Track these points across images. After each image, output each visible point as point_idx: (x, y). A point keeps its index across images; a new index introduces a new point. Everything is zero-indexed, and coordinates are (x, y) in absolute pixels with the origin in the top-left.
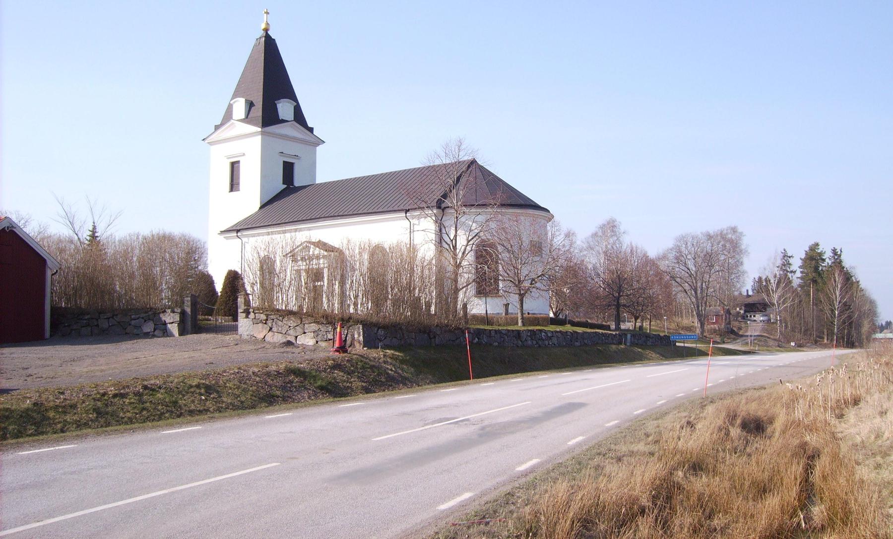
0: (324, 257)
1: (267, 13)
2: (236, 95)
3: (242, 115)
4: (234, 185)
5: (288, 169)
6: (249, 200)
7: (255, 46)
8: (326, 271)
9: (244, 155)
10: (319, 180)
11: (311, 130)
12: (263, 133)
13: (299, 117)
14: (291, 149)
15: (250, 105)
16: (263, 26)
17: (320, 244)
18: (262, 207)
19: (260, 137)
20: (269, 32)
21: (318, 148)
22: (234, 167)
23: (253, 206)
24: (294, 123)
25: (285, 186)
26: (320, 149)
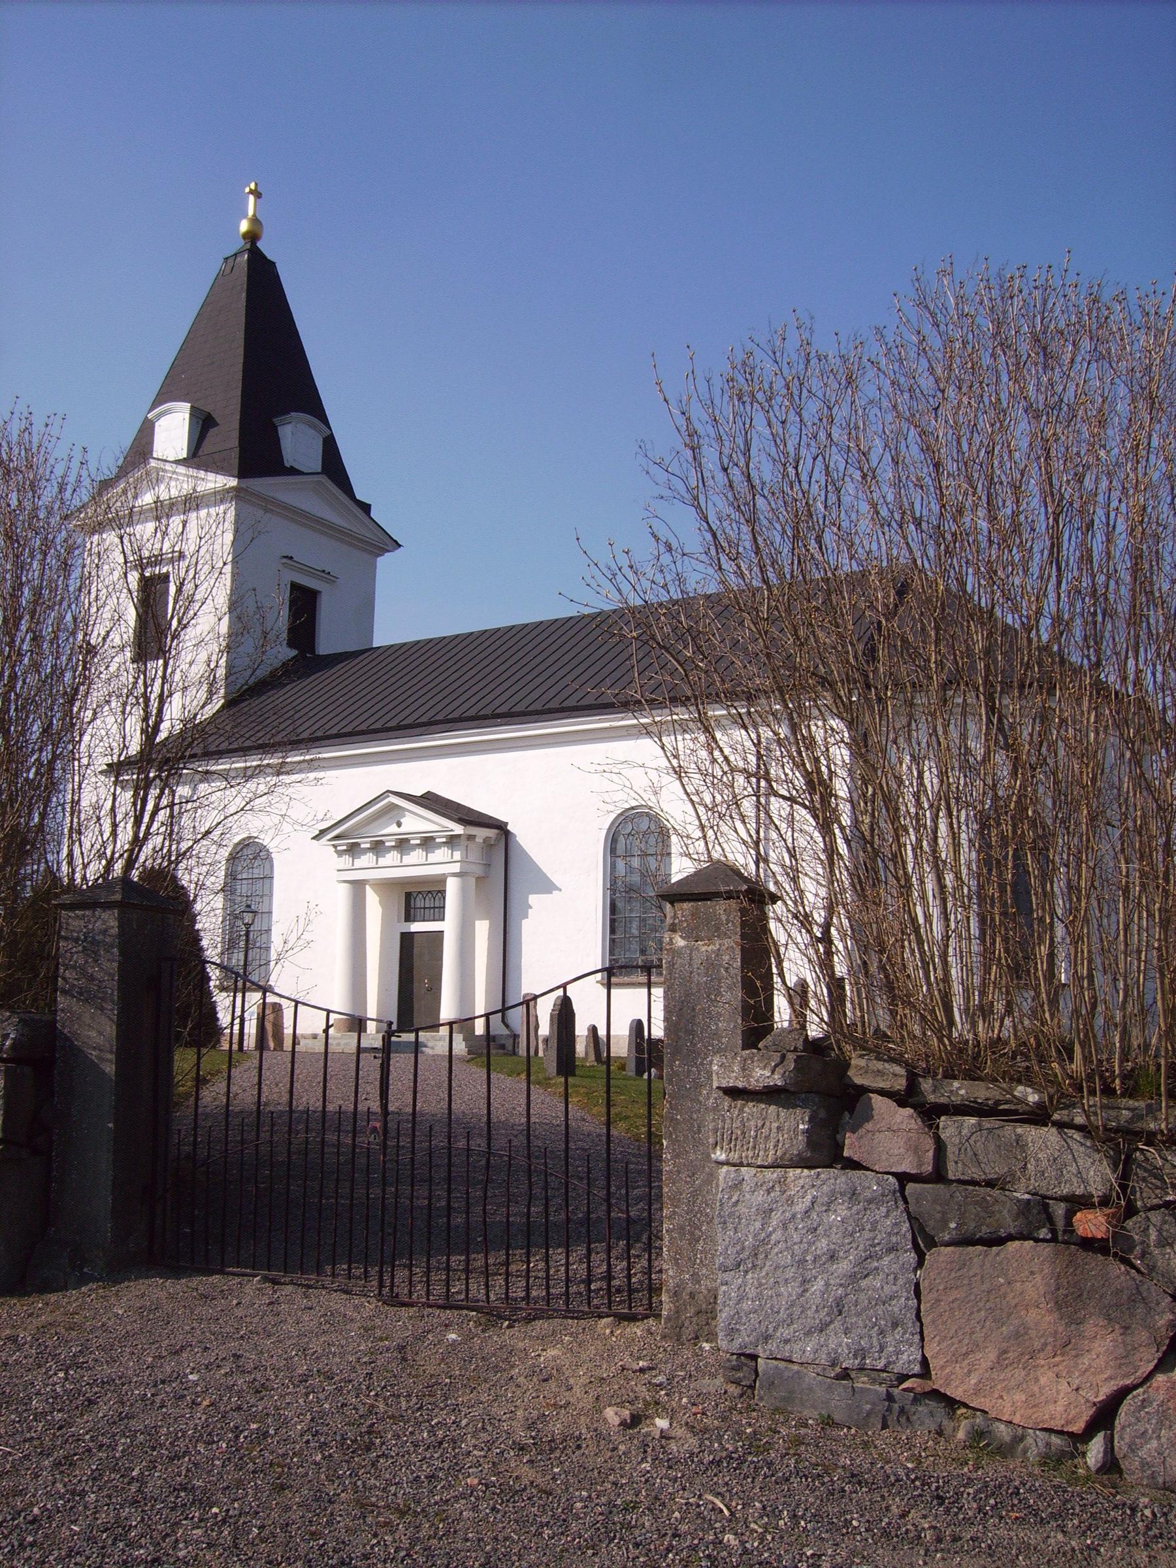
0: (452, 841)
1: (257, 194)
2: (166, 394)
3: (180, 448)
5: (304, 603)
7: (221, 275)
8: (452, 887)
10: (383, 637)
11: (366, 508)
12: (238, 495)
13: (333, 467)
14: (317, 552)
15: (203, 425)
16: (244, 226)
17: (431, 802)
19: (228, 512)
20: (260, 245)
24: (324, 479)
25: (294, 653)
26: (385, 563)
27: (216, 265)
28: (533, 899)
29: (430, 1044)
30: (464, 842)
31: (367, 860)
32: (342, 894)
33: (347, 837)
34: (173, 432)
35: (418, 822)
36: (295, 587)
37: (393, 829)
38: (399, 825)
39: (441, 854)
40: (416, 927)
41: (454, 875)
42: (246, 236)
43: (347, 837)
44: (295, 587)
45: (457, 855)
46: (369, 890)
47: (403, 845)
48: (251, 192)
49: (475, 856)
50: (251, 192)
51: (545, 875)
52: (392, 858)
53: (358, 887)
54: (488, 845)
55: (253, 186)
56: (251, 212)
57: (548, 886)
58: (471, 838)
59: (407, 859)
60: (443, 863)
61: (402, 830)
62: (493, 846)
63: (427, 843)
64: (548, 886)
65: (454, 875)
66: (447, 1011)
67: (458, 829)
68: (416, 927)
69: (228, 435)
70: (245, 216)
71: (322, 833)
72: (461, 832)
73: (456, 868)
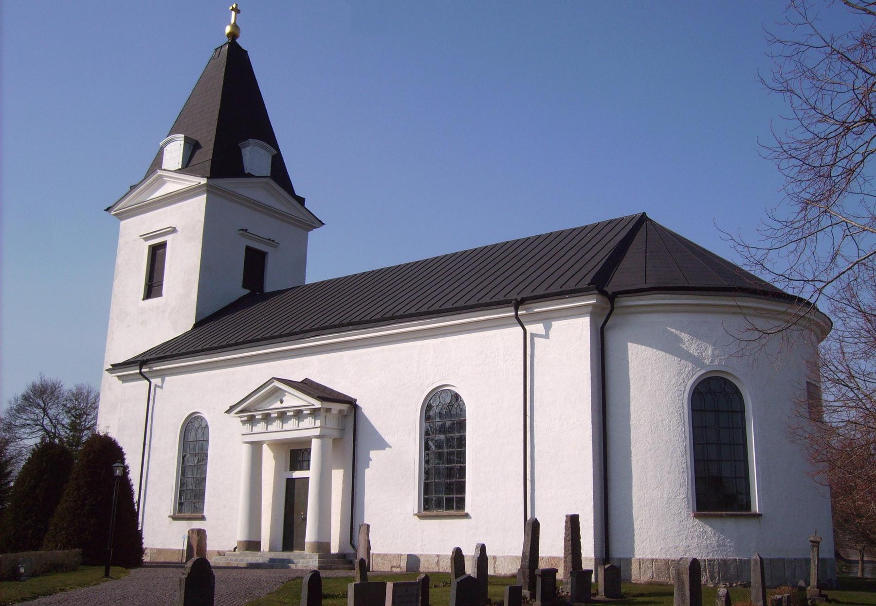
0: (314, 413)
1: (237, 11)
2: (174, 131)
4: (153, 288)
5: (255, 263)
6: (176, 311)
7: (213, 58)
8: (315, 445)
9: (174, 230)
11: (301, 201)
12: (209, 189)
13: (279, 174)
14: (263, 227)
15: (192, 148)
16: (228, 29)
17: (307, 387)
18: (196, 326)
20: (238, 41)
21: (311, 234)
22: (157, 254)
23: (185, 322)
25: (247, 292)
26: (314, 236)
27: (211, 53)
28: (373, 454)
29: (295, 561)
30: (323, 414)
31: (260, 427)
32: (244, 453)
33: (250, 411)
34: (174, 153)
35: (294, 399)
36: (249, 250)
37: (278, 405)
38: (282, 402)
39: (308, 422)
40: (297, 474)
41: (316, 437)
42: (229, 35)
43: (250, 411)
44: (249, 250)
45: (318, 423)
46: (265, 446)
47: (283, 416)
48: (233, 9)
49: (332, 422)
50: (233, 9)
51: (380, 436)
52: (276, 425)
53: (256, 447)
54: (342, 415)
55: (234, 6)
56: (233, 21)
57: (382, 444)
58: (328, 410)
59: (287, 426)
60: (308, 429)
61: (283, 405)
62: (345, 416)
63: (298, 414)
64: (382, 444)
65: (316, 437)
66: (310, 536)
67: (317, 404)
68: (297, 474)
69: (206, 153)
70: (229, 23)
71: (232, 408)
72: (319, 406)
73: (317, 432)
